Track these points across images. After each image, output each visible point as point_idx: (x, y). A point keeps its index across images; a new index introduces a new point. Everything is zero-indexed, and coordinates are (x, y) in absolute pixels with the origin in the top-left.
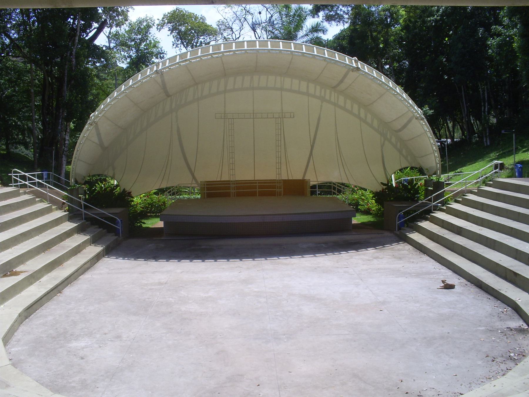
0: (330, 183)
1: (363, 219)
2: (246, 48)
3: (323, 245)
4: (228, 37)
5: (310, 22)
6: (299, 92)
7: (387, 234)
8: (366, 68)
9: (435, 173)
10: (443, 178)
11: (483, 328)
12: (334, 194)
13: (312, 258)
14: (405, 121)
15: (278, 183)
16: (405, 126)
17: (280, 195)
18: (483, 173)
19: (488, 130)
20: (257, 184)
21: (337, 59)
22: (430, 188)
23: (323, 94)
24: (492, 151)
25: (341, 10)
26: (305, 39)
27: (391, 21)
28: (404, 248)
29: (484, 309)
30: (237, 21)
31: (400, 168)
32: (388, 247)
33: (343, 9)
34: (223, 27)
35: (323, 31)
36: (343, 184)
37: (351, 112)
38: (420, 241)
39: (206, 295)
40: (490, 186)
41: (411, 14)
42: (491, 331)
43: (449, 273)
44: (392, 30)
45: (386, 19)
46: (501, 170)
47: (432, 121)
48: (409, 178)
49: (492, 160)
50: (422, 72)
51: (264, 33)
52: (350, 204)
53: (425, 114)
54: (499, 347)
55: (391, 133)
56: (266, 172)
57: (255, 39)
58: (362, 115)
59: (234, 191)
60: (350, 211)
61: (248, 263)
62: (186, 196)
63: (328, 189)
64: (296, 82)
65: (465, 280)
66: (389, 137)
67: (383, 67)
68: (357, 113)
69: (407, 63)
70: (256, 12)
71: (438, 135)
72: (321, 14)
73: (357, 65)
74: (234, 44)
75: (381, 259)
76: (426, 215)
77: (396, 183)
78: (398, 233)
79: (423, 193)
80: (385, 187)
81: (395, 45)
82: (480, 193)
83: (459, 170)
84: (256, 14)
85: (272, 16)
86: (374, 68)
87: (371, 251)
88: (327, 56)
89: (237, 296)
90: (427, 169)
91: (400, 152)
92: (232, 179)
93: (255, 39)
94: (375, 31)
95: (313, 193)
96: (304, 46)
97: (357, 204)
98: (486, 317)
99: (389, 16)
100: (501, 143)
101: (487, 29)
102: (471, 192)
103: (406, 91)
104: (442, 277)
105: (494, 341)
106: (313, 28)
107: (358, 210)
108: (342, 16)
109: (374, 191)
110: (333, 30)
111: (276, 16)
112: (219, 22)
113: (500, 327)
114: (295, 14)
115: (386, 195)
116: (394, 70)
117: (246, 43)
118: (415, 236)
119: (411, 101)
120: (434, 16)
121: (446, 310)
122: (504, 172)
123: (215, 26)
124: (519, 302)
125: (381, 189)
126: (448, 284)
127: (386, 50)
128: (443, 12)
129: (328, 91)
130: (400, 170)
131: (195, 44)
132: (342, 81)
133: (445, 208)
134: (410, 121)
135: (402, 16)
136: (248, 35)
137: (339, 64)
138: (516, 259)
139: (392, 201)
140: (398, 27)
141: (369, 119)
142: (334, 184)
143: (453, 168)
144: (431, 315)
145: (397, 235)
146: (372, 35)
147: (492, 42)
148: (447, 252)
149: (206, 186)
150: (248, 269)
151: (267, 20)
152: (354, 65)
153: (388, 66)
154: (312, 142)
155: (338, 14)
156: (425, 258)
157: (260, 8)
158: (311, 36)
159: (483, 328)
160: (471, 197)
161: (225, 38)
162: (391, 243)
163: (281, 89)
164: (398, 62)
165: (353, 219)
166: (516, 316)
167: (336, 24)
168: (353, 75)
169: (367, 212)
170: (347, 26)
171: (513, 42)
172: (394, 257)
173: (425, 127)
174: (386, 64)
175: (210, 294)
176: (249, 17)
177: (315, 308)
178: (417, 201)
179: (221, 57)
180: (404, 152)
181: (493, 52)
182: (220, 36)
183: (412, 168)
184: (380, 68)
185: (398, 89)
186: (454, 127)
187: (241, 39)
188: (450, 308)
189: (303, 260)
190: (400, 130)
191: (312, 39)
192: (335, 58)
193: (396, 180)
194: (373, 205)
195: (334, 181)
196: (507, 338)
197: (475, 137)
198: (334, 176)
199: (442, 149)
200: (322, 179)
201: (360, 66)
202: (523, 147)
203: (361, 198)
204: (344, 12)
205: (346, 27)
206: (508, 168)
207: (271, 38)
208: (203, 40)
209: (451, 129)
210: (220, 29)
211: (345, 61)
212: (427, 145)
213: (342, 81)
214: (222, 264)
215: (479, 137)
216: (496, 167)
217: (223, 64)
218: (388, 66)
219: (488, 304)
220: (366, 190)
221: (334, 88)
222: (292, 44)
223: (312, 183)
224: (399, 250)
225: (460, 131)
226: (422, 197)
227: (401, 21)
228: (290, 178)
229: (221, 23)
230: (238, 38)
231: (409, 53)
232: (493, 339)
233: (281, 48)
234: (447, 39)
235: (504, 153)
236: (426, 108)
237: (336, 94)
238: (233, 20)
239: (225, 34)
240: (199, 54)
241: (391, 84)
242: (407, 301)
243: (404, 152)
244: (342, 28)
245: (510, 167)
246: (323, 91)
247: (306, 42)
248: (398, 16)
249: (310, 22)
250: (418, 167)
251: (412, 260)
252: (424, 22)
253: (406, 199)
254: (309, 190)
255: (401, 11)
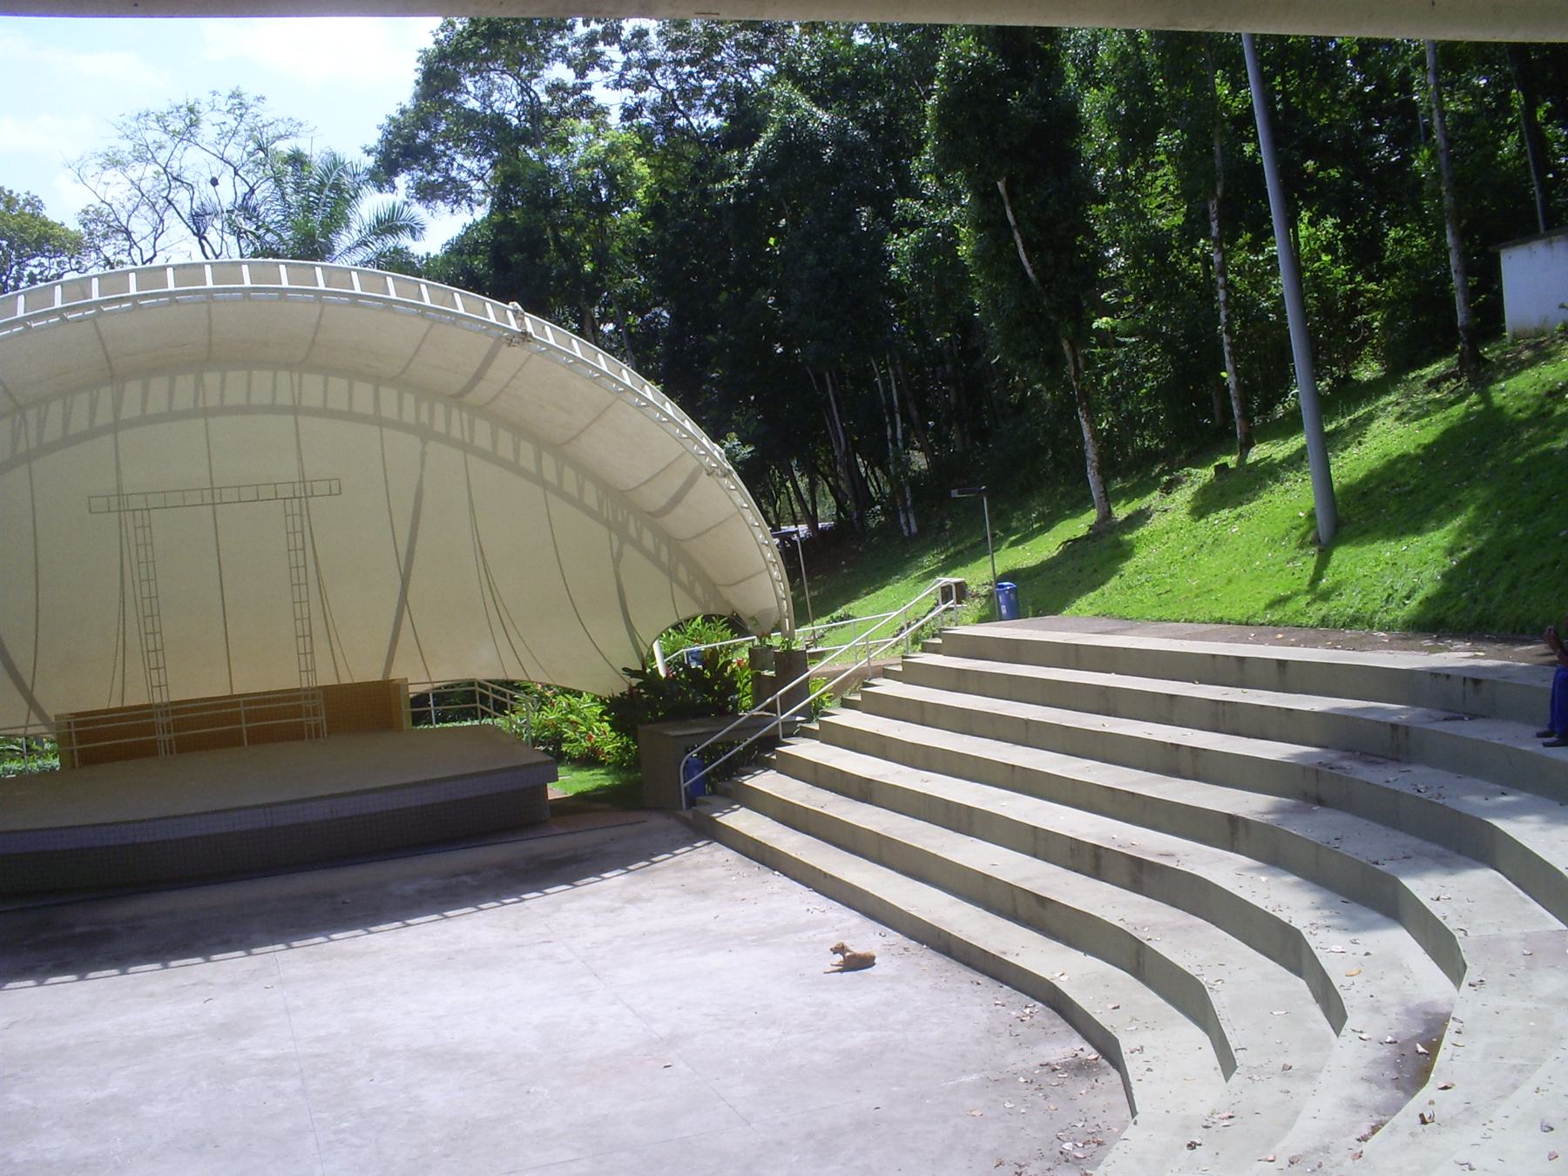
0: (471, 683)
1: (580, 782)
2: (171, 287)
3: (465, 878)
4: (119, 257)
5: (371, 204)
6: (350, 416)
7: (657, 821)
8: (549, 333)
9: (778, 627)
10: (802, 637)
11: (974, 1077)
12: (485, 714)
13: (436, 926)
14: (678, 482)
15: (306, 697)
16: (676, 500)
17: (317, 736)
18: (911, 615)
19: (908, 489)
20: (242, 709)
21: (461, 310)
22: (766, 673)
23: (424, 418)
24: (925, 550)
25: (461, 167)
26: (361, 254)
27: (610, 196)
28: (710, 859)
29: (967, 1017)
30: (144, 209)
31: (675, 620)
32: (664, 861)
33: (467, 164)
34: (101, 229)
35: (413, 231)
36: (509, 684)
37: (515, 468)
38: (756, 834)
39: (101, 1094)
40: (935, 650)
41: (667, 174)
42: (999, 1081)
43: (852, 919)
44: (614, 221)
45: (596, 190)
46: (959, 602)
47: (754, 475)
48: (702, 648)
49: (931, 575)
50: (710, 338)
51: (232, 240)
52: (535, 741)
53: (730, 455)
54: (1029, 1130)
55: (632, 519)
56: (265, 668)
57: (202, 259)
58: (550, 475)
59: (167, 737)
60: (536, 764)
61: (230, 966)
62: (15, 765)
63: (466, 699)
64: (338, 385)
65: (901, 937)
66: (632, 531)
67: (596, 330)
68: (533, 469)
69: (665, 314)
70: (202, 179)
71: (771, 514)
72: (402, 180)
73: (523, 324)
74: (132, 276)
75: (649, 900)
76: (763, 752)
77: (668, 665)
78: (689, 814)
79: (748, 689)
80: (635, 681)
81: (629, 264)
82: (912, 674)
83: (840, 612)
84: (202, 186)
85: (252, 191)
86: (572, 331)
87: (614, 881)
88: (427, 302)
89: (204, 1084)
90: (753, 618)
91: (671, 574)
92: (158, 701)
93: (199, 258)
94: (565, 226)
95: (418, 719)
96: (354, 274)
97: (558, 739)
98: (978, 1042)
99: (604, 183)
100: (949, 524)
101: (883, 209)
102: (886, 673)
103: (669, 392)
104: (833, 935)
105: (1010, 1112)
106: (379, 221)
107: (560, 758)
108: (465, 184)
109: (606, 694)
110: (441, 228)
111: (265, 190)
112: (86, 212)
113: (1021, 1065)
114: (322, 183)
115: (642, 706)
116: (630, 336)
117: (170, 271)
118: (740, 820)
119: (689, 425)
120: (731, 177)
121: (859, 1038)
122: (972, 608)
123: (73, 225)
124: (1063, 984)
125: (626, 690)
126: (854, 956)
127: (601, 280)
128: (756, 164)
129: (440, 409)
130: (675, 627)
131: (11, 282)
132: (478, 377)
133: (816, 726)
134: (690, 482)
135: (641, 179)
136: (179, 246)
137: (466, 323)
138: (1035, 856)
139: (659, 720)
140: (631, 213)
141: (570, 486)
142: (481, 685)
143: (823, 606)
144: (817, 1057)
145: (687, 823)
146: (557, 238)
147: (900, 244)
148: (836, 854)
149: (73, 730)
150: (234, 985)
151: (239, 201)
152: (514, 326)
153: (611, 327)
154: (402, 562)
155: (453, 180)
156: (778, 881)
157: (213, 168)
158: (377, 246)
159: (974, 1077)
160: (886, 687)
161: (107, 260)
162: (670, 847)
163: (296, 410)
164: (640, 312)
165: (549, 785)
166: (1060, 1025)
167: (448, 208)
168: (510, 356)
169: (589, 760)
170: (481, 213)
171: (958, 241)
172: (686, 890)
173: (735, 496)
174: (605, 319)
175: (114, 1087)
176: (181, 196)
177: (462, 1089)
178: (734, 715)
179: (93, 318)
180: (682, 573)
181: (903, 271)
182: (93, 255)
183: (707, 618)
184: (589, 331)
185: (651, 391)
186: (812, 491)
187: (157, 262)
188: (870, 1028)
189: (407, 933)
190: (664, 511)
191: (381, 255)
192: (455, 306)
193: (665, 656)
194: (605, 737)
195: (481, 674)
196: (1046, 1097)
197: (875, 514)
198: (481, 663)
199: (788, 551)
200: (446, 672)
201: (530, 329)
202: (1008, 531)
203: (568, 720)
204: (470, 173)
205: (479, 219)
206: (977, 595)
207: (255, 254)
208: (36, 271)
209: (806, 497)
210: (90, 234)
211: (486, 314)
212: (743, 542)
213: (478, 377)
214: (147, 977)
215: (884, 512)
216: (946, 593)
217: (100, 338)
218: (611, 327)
219: (977, 1000)
220: (579, 695)
221: (457, 398)
222: (318, 270)
223: (414, 690)
224: (697, 867)
225: (831, 499)
226: (747, 701)
227: (639, 194)
228: (346, 680)
229: (92, 216)
230: (151, 260)
231: (668, 285)
232: (1008, 1105)
233: (285, 284)
234: (772, 241)
235: (961, 552)
236: (733, 440)
237: (465, 415)
238: (129, 206)
239: (108, 251)
240: (21, 313)
241: (628, 376)
242: (742, 1023)
243: (682, 573)
244: (469, 221)
245: (983, 591)
246: (424, 407)
247: (366, 263)
248: (628, 179)
249: (371, 204)
250: (727, 612)
251: (739, 895)
252: (705, 195)
253: (701, 712)
254: (407, 711)
255: (636, 166)
